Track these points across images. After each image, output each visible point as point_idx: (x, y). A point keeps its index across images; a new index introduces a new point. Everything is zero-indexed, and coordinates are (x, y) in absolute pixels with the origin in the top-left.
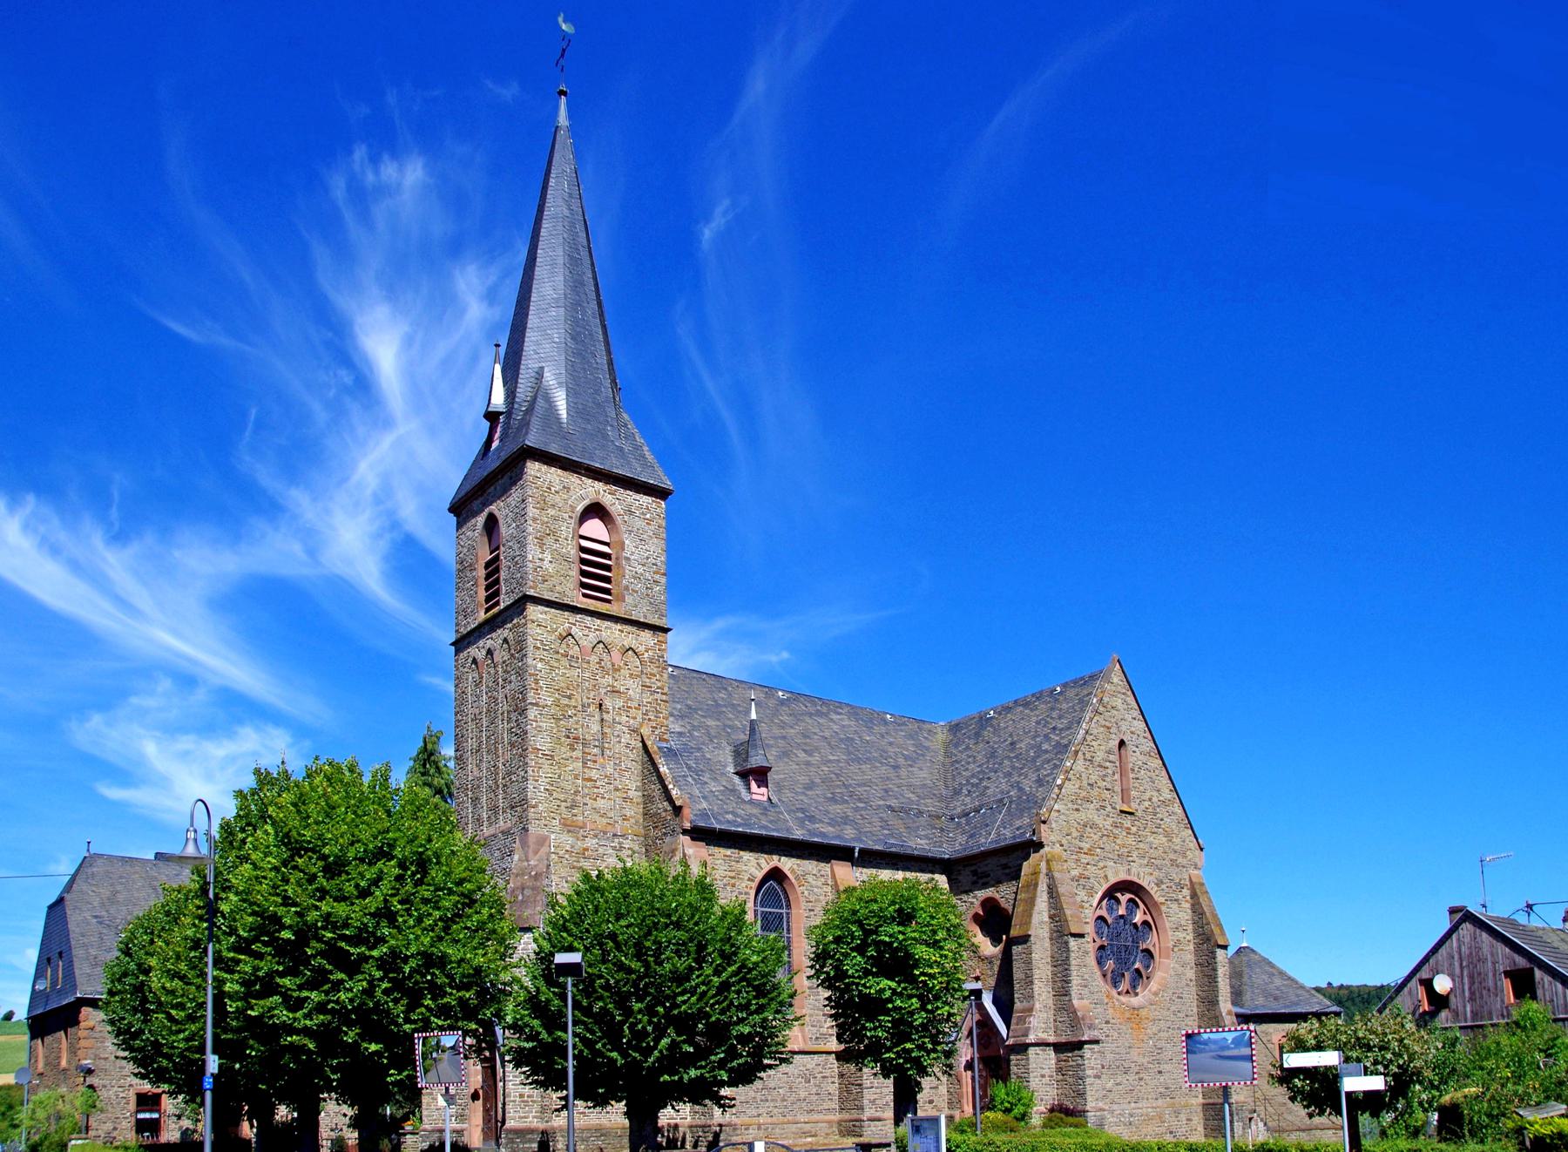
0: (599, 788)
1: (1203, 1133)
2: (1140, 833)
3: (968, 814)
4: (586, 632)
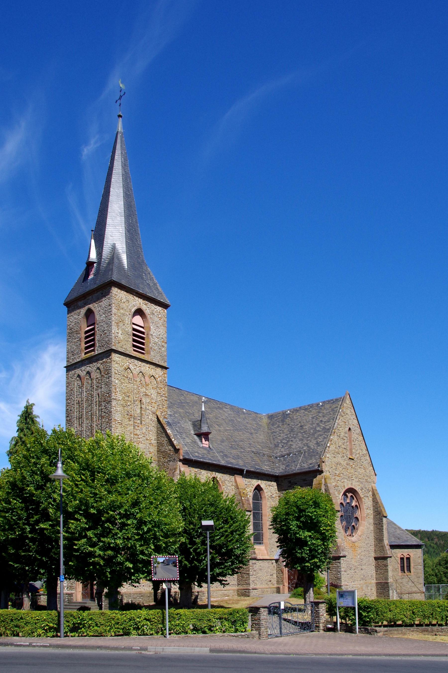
0: (140, 438)
1: (376, 595)
2: (356, 468)
3: (283, 456)
4: (135, 367)
